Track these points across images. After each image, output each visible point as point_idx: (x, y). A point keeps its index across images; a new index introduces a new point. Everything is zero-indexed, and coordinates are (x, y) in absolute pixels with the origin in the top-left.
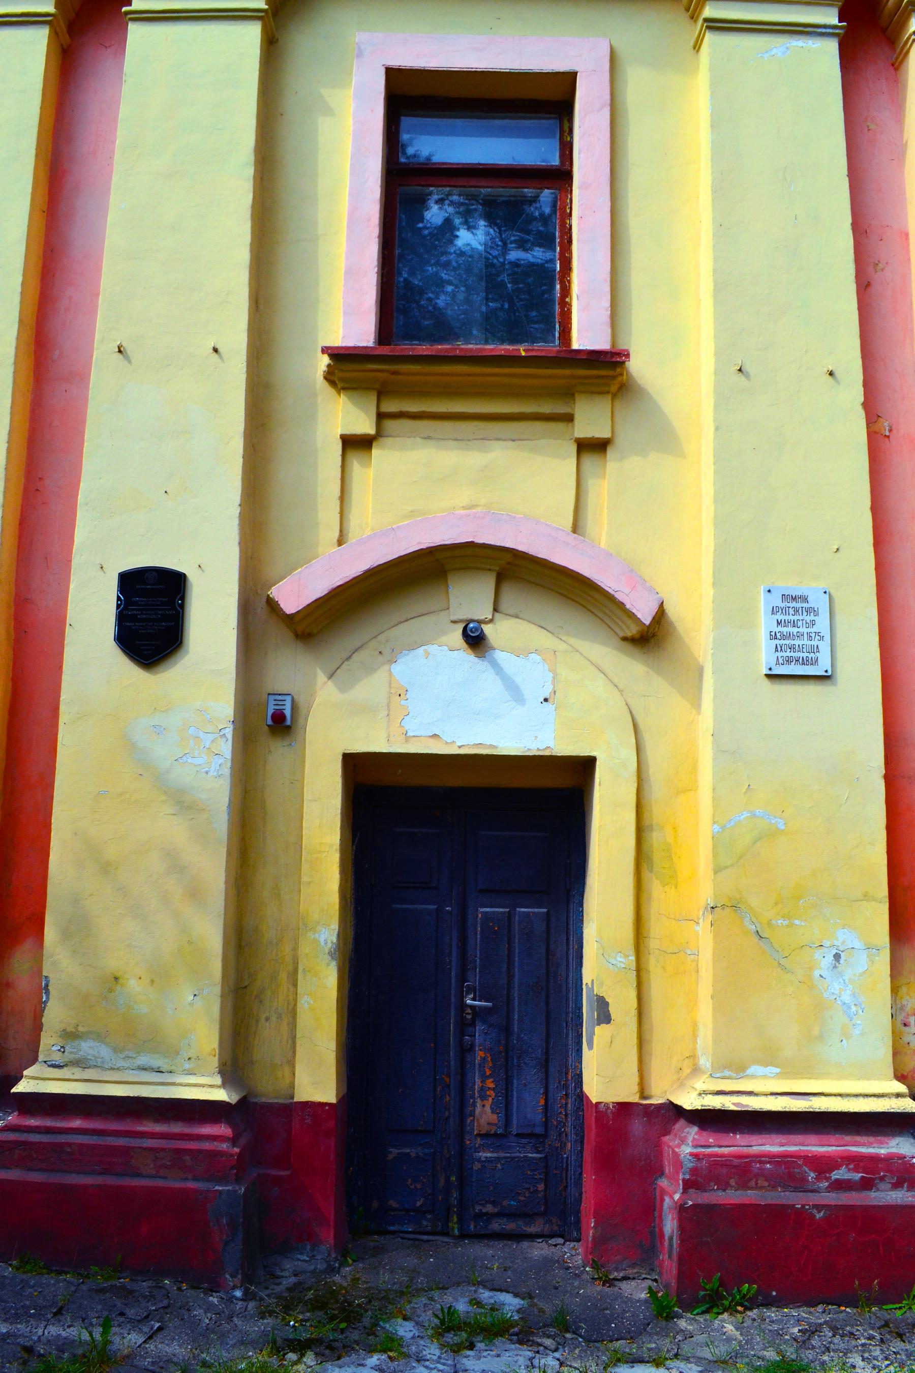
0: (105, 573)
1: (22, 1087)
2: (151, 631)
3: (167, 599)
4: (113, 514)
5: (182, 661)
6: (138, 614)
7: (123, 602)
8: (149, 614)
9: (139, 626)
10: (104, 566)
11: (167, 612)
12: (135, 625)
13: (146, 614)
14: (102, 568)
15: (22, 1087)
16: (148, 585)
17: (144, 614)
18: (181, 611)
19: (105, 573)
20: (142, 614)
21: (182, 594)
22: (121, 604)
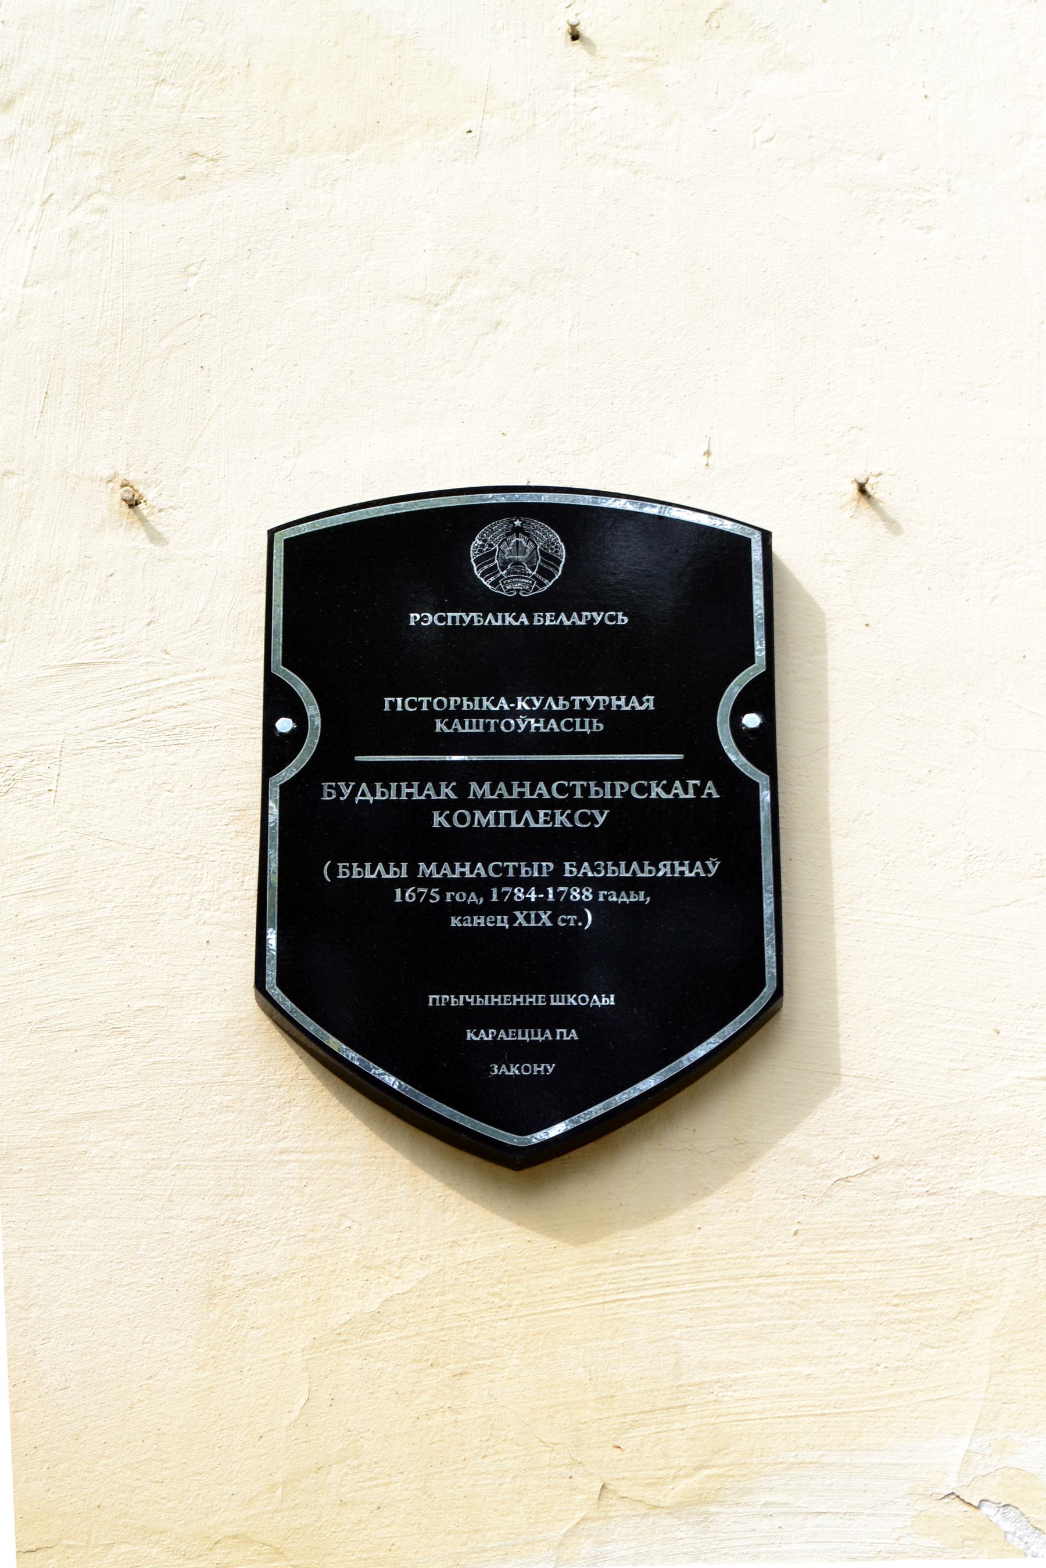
0: (155, 537)
1: (449, 826)
2: (561, 819)
3: (649, 703)
4: (199, 167)
5: (794, 1140)
6: (442, 805)
7: (313, 711)
8: (521, 805)
9: (445, 884)
10: (149, 494)
11: (657, 791)
12: (414, 879)
13: (501, 804)
14: (133, 504)
15: (449, 826)
16: (500, 604)
17: (484, 805)
18: (762, 779)
19: (155, 537)
20: (464, 801)
21: (767, 992)
22: (298, 737)
